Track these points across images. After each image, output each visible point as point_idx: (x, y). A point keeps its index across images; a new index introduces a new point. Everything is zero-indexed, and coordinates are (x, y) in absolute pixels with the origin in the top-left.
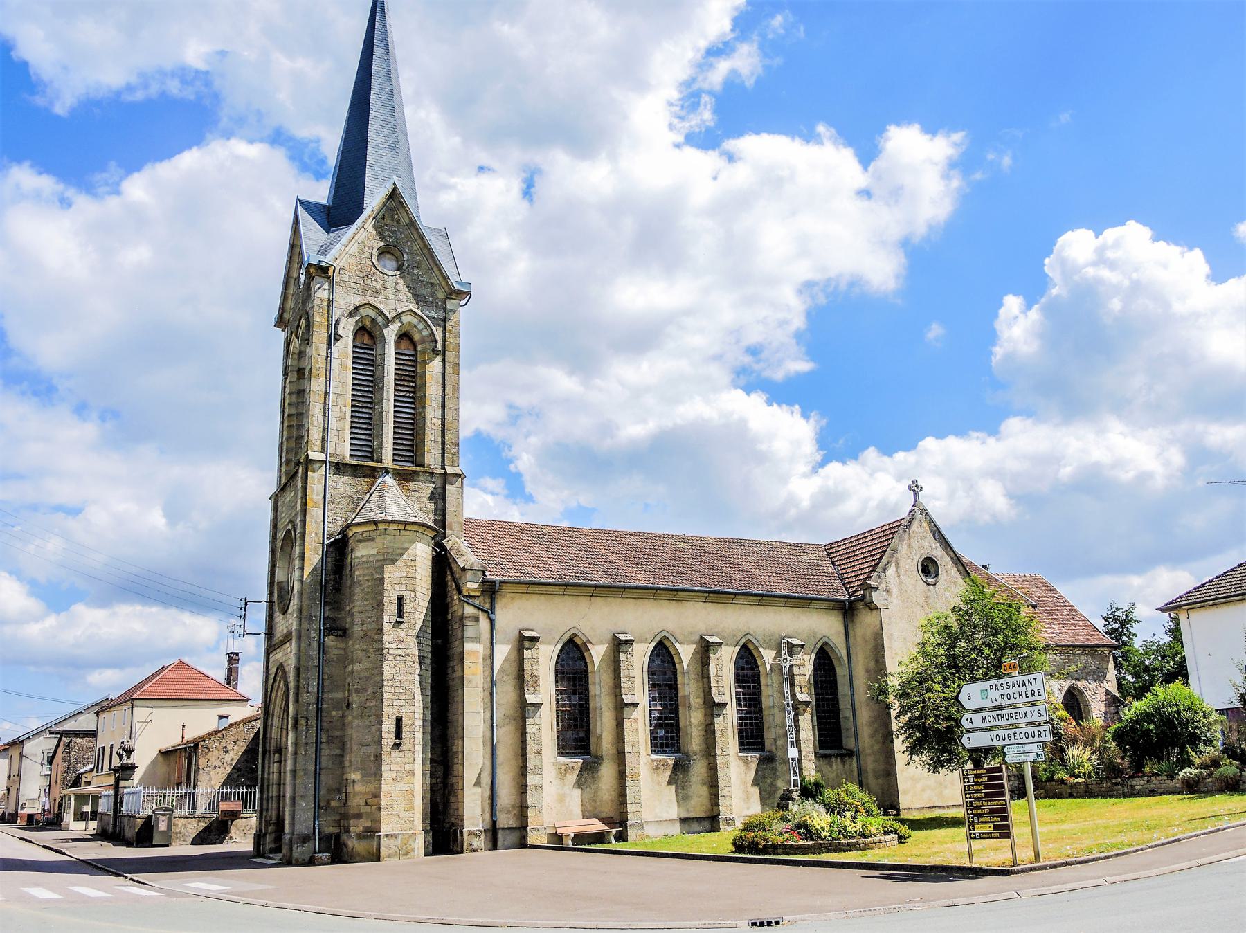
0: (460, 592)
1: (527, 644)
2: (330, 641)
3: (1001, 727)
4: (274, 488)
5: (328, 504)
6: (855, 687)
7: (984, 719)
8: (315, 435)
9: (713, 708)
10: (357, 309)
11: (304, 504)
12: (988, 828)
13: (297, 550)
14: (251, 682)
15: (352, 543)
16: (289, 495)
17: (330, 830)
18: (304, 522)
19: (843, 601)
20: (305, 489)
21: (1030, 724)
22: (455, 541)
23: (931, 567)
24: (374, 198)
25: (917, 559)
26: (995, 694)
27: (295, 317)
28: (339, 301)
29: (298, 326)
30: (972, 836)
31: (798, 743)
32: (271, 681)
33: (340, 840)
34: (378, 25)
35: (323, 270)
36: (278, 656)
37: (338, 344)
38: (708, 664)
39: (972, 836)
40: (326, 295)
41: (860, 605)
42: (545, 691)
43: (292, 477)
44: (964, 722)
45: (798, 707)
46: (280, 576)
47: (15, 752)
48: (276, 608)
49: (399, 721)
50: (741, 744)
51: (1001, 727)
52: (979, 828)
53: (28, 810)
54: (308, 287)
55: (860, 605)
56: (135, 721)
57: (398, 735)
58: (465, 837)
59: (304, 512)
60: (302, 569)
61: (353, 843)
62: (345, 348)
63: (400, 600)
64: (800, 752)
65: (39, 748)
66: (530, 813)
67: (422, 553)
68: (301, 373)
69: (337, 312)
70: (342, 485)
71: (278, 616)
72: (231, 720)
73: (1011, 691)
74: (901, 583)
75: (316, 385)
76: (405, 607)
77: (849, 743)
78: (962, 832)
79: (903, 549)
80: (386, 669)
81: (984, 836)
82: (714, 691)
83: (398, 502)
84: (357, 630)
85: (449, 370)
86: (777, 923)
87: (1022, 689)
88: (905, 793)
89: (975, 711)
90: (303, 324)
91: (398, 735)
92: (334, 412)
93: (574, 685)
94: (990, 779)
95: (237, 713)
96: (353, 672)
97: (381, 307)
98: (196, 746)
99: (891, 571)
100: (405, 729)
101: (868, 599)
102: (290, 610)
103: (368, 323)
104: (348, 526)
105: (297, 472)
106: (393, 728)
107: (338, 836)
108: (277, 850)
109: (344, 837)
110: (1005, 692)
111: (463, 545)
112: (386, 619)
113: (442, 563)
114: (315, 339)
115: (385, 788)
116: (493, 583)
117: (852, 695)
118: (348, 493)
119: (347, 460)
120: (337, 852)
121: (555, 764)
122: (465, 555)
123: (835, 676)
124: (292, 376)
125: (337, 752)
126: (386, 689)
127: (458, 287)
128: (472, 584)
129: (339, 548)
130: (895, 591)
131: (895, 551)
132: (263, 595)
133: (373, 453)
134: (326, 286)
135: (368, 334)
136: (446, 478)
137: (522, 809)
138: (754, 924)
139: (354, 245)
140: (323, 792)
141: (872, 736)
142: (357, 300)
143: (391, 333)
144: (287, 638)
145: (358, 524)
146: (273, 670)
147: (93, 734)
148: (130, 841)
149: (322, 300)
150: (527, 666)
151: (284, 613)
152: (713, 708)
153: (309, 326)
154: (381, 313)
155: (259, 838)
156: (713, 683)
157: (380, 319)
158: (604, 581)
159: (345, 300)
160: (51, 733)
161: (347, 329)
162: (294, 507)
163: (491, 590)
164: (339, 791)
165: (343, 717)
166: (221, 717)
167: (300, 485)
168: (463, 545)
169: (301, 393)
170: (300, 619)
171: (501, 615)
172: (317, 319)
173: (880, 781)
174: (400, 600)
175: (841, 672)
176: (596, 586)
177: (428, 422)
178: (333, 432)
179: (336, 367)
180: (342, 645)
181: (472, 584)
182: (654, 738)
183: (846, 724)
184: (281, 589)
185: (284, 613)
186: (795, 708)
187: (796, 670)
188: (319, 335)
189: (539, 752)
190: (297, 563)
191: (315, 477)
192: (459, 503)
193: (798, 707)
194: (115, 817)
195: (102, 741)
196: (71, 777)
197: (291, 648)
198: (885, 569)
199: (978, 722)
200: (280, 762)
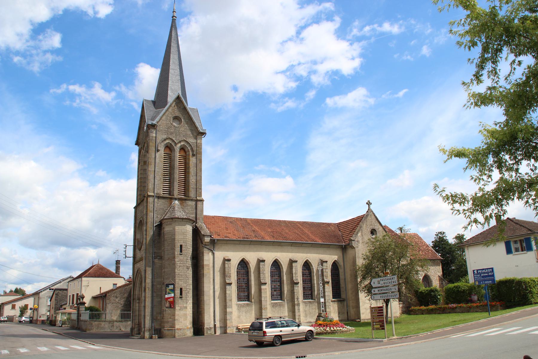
0: (202, 244)
1: (226, 262)
2: (156, 261)
3: (383, 293)
4: (135, 205)
5: (156, 211)
6: (345, 275)
7: (378, 291)
8: (151, 186)
9: (294, 284)
10: (165, 140)
11: (147, 211)
12: (379, 326)
13: (145, 228)
14: (127, 271)
15: (164, 225)
16: (141, 208)
17: (157, 327)
18: (147, 218)
19: (342, 245)
20: (147, 206)
21: (392, 292)
22: (201, 224)
23: (374, 232)
24: (171, 97)
25: (369, 230)
26: (382, 282)
27: (142, 141)
28: (158, 137)
29: (144, 146)
30: (373, 329)
31: (324, 297)
32: (135, 274)
33: (161, 331)
34: (173, 34)
35: (153, 126)
36: (138, 265)
37: (158, 153)
38: (292, 269)
39: (373, 329)
40: (154, 135)
41: (348, 247)
42: (233, 278)
43: (143, 201)
44: (372, 291)
45: (324, 283)
46: (138, 236)
47: (37, 297)
48: (137, 248)
49: (181, 289)
50: (304, 297)
51: (383, 293)
52: (375, 326)
53: (42, 319)
54: (147, 132)
55: (348, 247)
56: (83, 285)
57: (181, 294)
58: (205, 330)
59: (147, 214)
60: (146, 239)
61: (166, 332)
62: (161, 155)
63: (181, 246)
64: (325, 300)
65: (46, 295)
66: (228, 322)
67: (189, 228)
68: (145, 163)
69: (158, 141)
70: (160, 204)
71: (137, 251)
72: (118, 286)
73: (387, 281)
74: (362, 239)
75: (151, 168)
76: (183, 249)
77: (343, 296)
78: (370, 328)
79: (364, 226)
80: (176, 271)
81: (377, 329)
82: (294, 279)
83: (179, 210)
84: (166, 257)
85: (198, 162)
86: (304, 357)
87: (390, 281)
88: (363, 314)
89: (376, 288)
90: (146, 145)
91: (181, 294)
92: (157, 178)
93: (499, 97)
94: (379, 310)
95: (120, 282)
96: (164, 272)
97: (174, 139)
98: (106, 295)
99: (359, 234)
100: (183, 292)
101: (351, 245)
102: (142, 249)
103: (169, 145)
104: (162, 220)
105: (144, 199)
106: (179, 292)
107: (160, 330)
108: (139, 334)
109: (163, 330)
110: (385, 281)
111: (204, 226)
112: (176, 253)
113: (196, 232)
114: (150, 151)
115: (177, 313)
116: (214, 240)
117: (345, 279)
118: (162, 207)
119: (162, 195)
120: (493, 271)
121: (237, 304)
122: (205, 230)
123: (339, 272)
124: (142, 163)
125: (160, 300)
126: (176, 278)
127: (201, 131)
128: (207, 239)
129: (160, 226)
130: (361, 241)
131: (361, 227)
132: (132, 243)
133: (171, 192)
134: (155, 132)
135: (169, 148)
136: (197, 201)
137: (224, 321)
138: (297, 357)
139: (163, 118)
140: (155, 314)
141: (352, 294)
142: (165, 137)
143: (177, 148)
144: (141, 259)
145: (166, 219)
146: (136, 270)
147: (66, 290)
148: (78, 330)
149: (153, 137)
150: (226, 270)
151: (140, 250)
152: (294, 284)
153: (148, 147)
154: (173, 141)
155: (132, 329)
156: (294, 275)
157: (173, 144)
158: (254, 239)
159: (161, 137)
160: (50, 289)
161: (162, 148)
162: (143, 212)
163: (213, 242)
164: (160, 313)
165: (161, 288)
166: (114, 284)
167: (145, 204)
168: (204, 226)
169: (145, 170)
170: (146, 253)
171: (217, 253)
172: (151, 144)
173: (354, 310)
174: (181, 246)
175: (341, 271)
176: (251, 241)
177: (191, 181)
178: (156, 185)
179: (158, 158)
180: (160, 262)
181: (207, 239)
182: (272, 295)
183: (342, 290)
184: (138, 241)
185: (140, 250)
186: (324, 285)
187: (324, 270)
188: (152, 149)
189: (231, 300)
190: (144, 233)
191: (151, 200)
192: (202, 211)
193: (324, 283)
194: (78, 321)
195: (70, 293)
196: (59, 306)
197: (143, 263)
198: (357, 233)
199: (377, 292)
200: (139, 303)
